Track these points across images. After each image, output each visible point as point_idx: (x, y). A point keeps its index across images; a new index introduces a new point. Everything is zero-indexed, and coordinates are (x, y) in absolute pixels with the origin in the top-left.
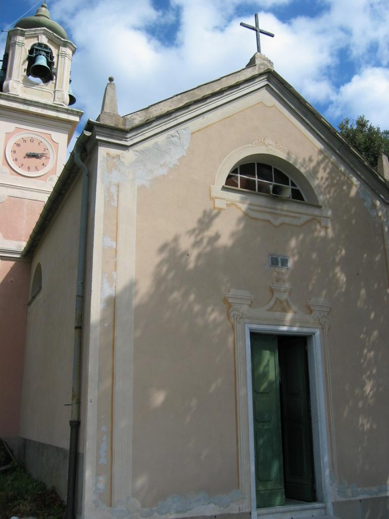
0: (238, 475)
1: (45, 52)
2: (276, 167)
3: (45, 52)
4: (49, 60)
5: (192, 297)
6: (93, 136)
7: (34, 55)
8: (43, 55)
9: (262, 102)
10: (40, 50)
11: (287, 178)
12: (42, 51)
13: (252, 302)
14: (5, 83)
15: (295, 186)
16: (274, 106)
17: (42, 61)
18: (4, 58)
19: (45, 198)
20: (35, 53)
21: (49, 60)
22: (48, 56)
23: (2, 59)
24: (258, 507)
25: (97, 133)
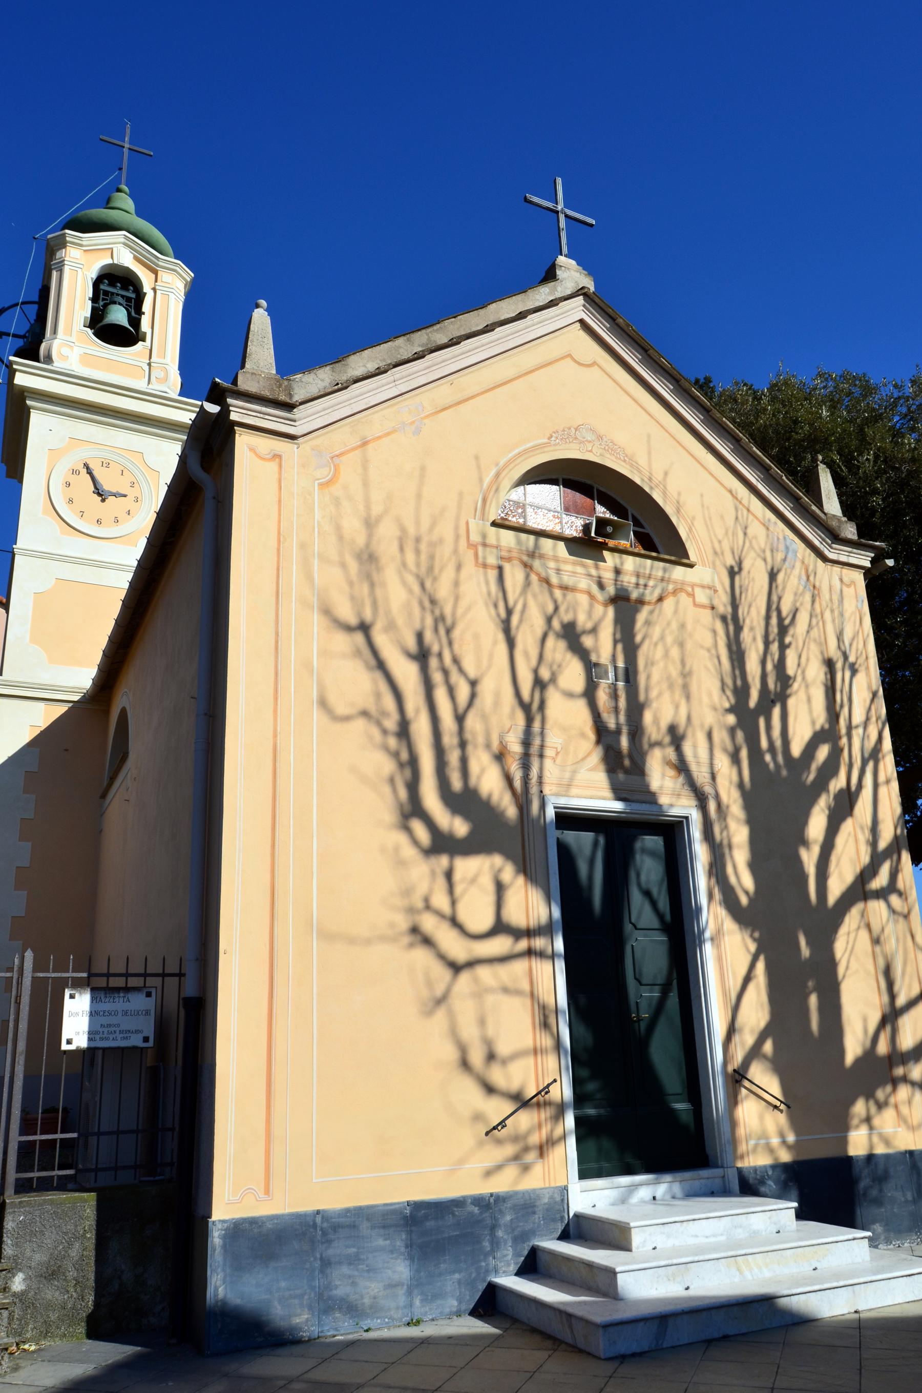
0: (547, 853)
1: (123, 296)
2: (601, 489)
3: (123, 296)
4: (133, 314)
5: (417, 1302)
6: (225, 411)
7: (101, 303)
8: (120, 304)
9: (570, 356)
10: (113, 294)
11: (626, 511)
12: (118, 295)
13: (557, 753)
14: (43, 346)
15: (642, 527)
16: (594, 364)
17: (118, 315)
18: (40, 296)
19: (122, 581)
20: (103, 299)
21: (133, 314)
22: (130, 307)
23: (36, 299)
24: (584, 1174)
25: (231, 408)
